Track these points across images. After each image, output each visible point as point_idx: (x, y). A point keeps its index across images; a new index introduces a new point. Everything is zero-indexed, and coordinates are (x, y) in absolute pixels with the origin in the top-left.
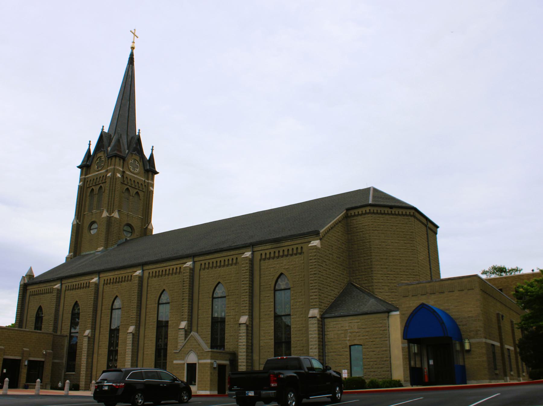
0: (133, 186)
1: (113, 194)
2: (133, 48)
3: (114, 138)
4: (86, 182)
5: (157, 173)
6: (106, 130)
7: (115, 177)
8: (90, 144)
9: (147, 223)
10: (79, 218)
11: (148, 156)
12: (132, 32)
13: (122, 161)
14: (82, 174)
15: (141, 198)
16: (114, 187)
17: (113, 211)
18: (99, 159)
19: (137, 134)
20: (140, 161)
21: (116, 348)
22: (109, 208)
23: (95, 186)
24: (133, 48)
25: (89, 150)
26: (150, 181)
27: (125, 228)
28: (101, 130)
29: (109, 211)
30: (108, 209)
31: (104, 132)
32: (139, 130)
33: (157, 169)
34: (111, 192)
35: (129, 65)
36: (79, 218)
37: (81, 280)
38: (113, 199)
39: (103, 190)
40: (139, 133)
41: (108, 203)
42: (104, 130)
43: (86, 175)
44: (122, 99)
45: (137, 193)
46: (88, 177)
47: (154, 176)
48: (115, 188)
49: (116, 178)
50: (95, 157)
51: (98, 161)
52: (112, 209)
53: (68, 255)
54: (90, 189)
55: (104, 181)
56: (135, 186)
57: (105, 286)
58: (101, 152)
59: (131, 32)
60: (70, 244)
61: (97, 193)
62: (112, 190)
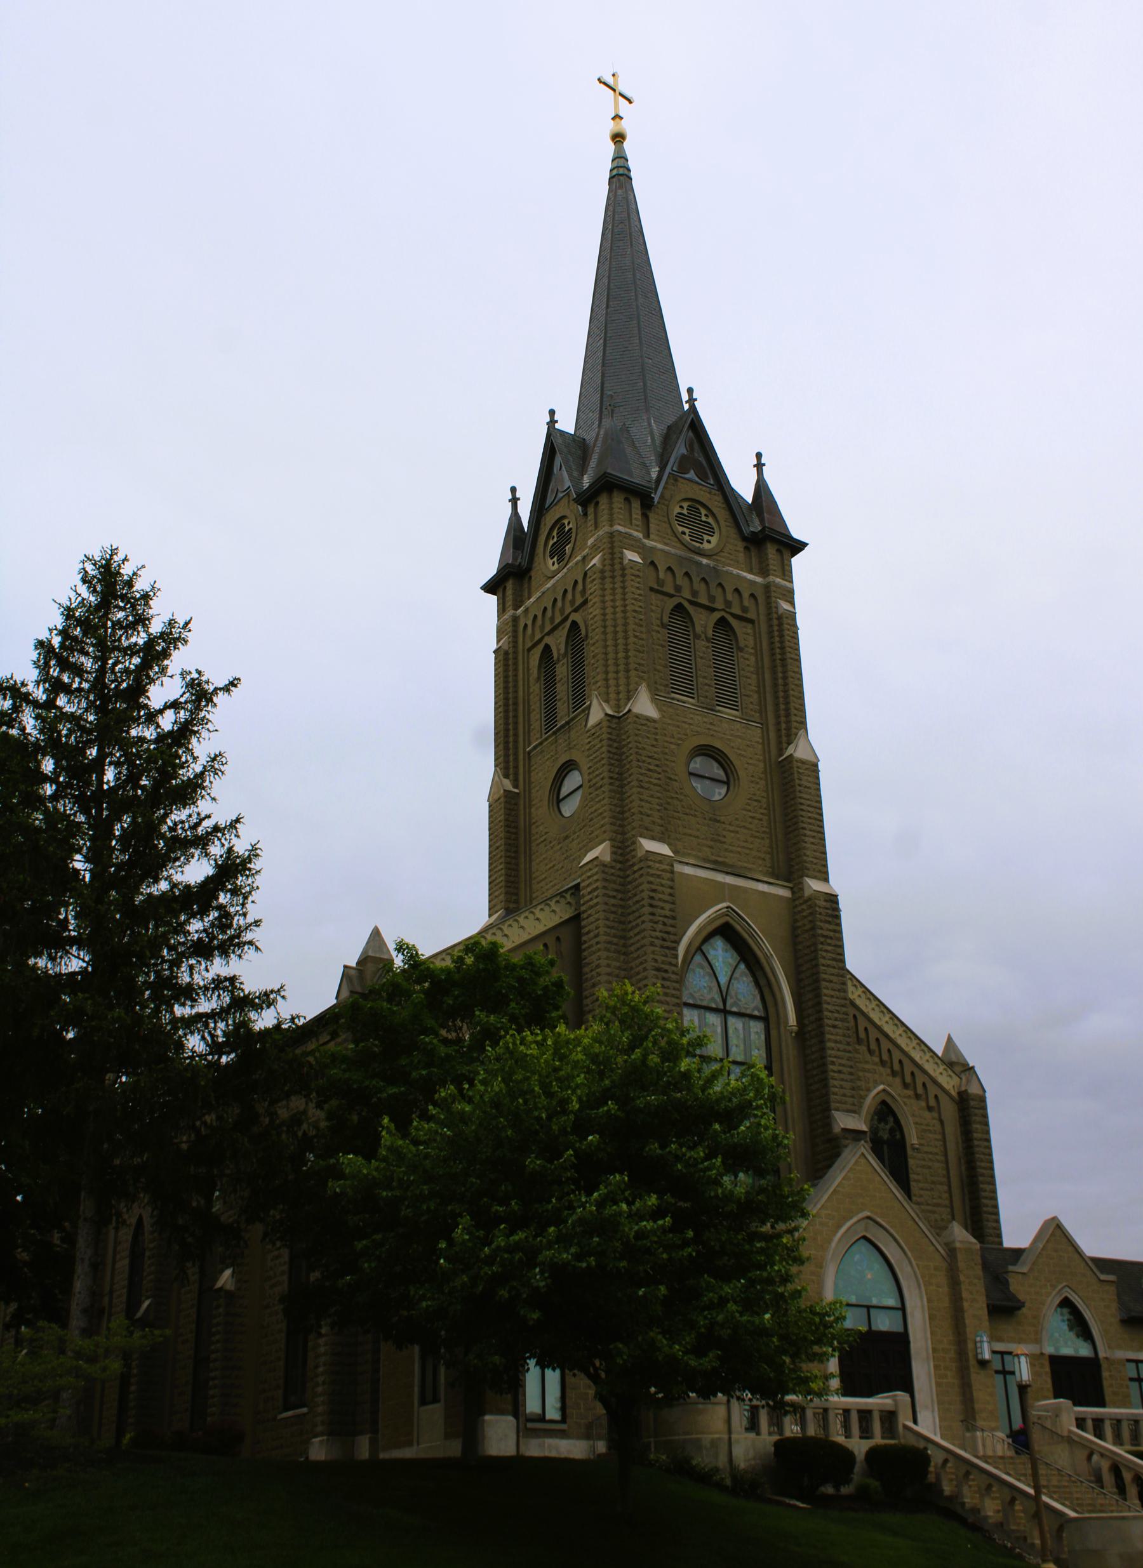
0: (703, 600)
2: (618, 138)
5: (797, 547)
6: (567, 424)
8: (514, 501)
11: (747, 492)
12: (605, 84)
13: (636, 505)
14: (502, 609)
15: (742, 644)
18: (555, 533)
19: (686, 407)
21: (781, 751)
24: (618, 138)
25: (515, 516)
27: (698, 764)
29: (612, 696)
32: (690, 391)
33: (796, 531)
39: (583, 632)
40: (692, 401)
42: (557, 426)
43: (516, 608)
45: (722, 623)
47: (790, 566)
49: (623, 569)
50: (542, 526)
51: (555, 540)
54: (537, 652)
55: (579, 601)
56: (712, 598)
59: (602, 85)
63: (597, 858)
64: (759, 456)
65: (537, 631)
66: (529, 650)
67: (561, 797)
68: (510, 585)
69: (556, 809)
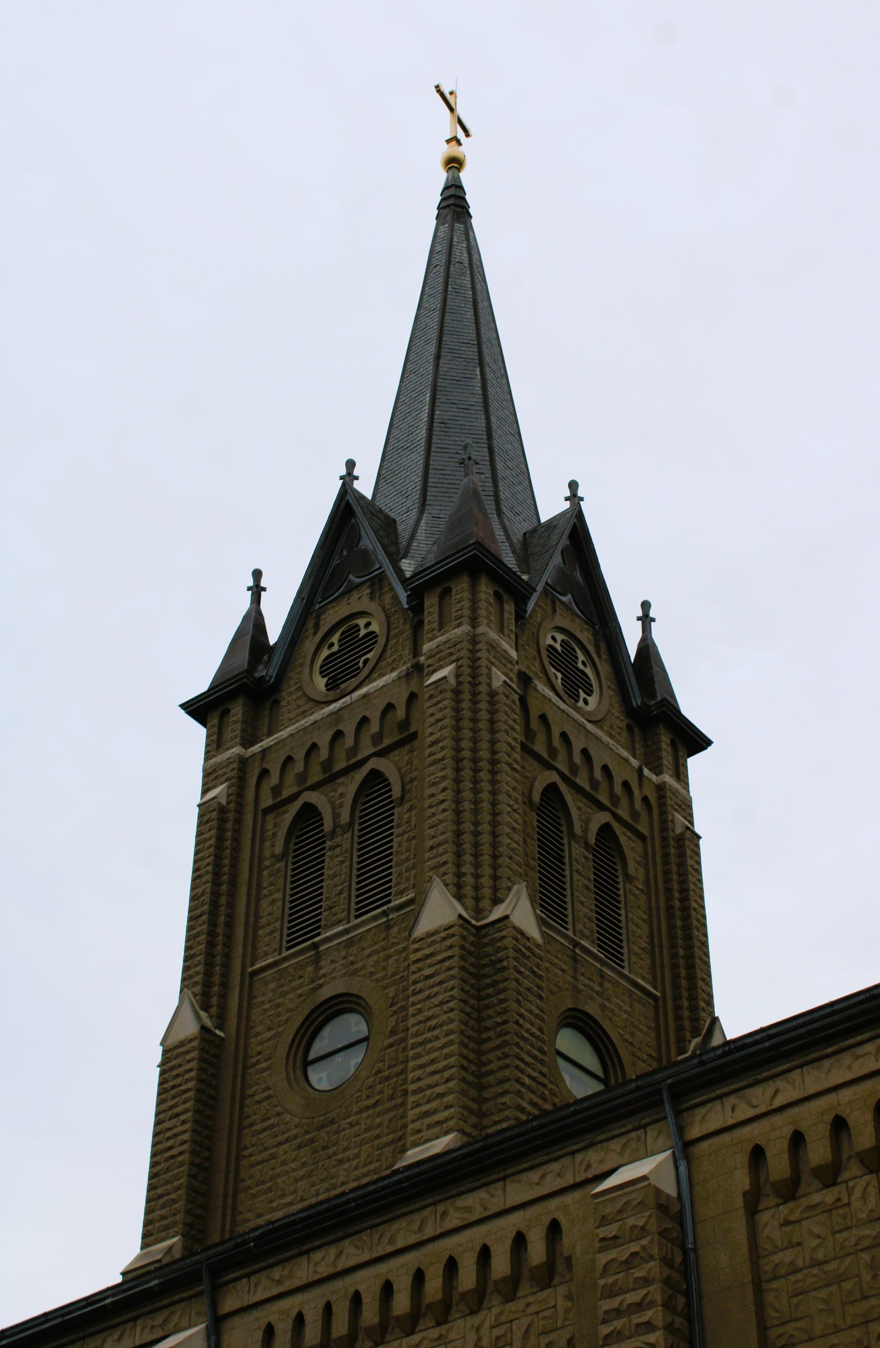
1: (486, 786)
2: (454, 164)
3: (421, 534)
4: (252, 781)
7: (483, 688)
8: (257, 590)
9: (695, 1032)
10: (214, 1001)
14: (214, 746)
16: (484, 745)
17: (495, 889)
18: (335, 639)
20: (597, 648)
22: (467, 869)
23: (327, 788)
24: (454, 164)
26: (667, 778)
28: (337, 485)
29: (468, 890)
30: (459, 875)
31: (355, 492)
34: (467, 774)
35: (445, 228)
36: (214, 1001)
37: (449, 1224)
38: (486, 817)
41: (458, 844)
43: (247, 743)
44: (438, 357)
46: (264, 752)
47: (686, 767)
48: (494, 753)
51: (335, 648)
52: (486, 881)
53: (139, 1258)
57: (764, 1217)
58: (349, 591)
59: (438, 96)
60: (152, 1176)
61: (345, 818)
62: (475, 761)
63: (644, 1178)
64: (257, 574)
65: (290, 777)
66: (267, 811)
67: (312, 1056)
68: (237, 711)
69: (299, 1073)
